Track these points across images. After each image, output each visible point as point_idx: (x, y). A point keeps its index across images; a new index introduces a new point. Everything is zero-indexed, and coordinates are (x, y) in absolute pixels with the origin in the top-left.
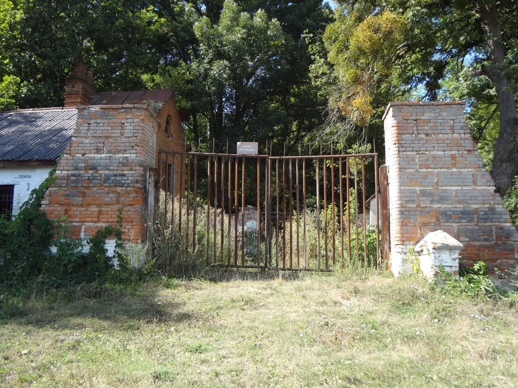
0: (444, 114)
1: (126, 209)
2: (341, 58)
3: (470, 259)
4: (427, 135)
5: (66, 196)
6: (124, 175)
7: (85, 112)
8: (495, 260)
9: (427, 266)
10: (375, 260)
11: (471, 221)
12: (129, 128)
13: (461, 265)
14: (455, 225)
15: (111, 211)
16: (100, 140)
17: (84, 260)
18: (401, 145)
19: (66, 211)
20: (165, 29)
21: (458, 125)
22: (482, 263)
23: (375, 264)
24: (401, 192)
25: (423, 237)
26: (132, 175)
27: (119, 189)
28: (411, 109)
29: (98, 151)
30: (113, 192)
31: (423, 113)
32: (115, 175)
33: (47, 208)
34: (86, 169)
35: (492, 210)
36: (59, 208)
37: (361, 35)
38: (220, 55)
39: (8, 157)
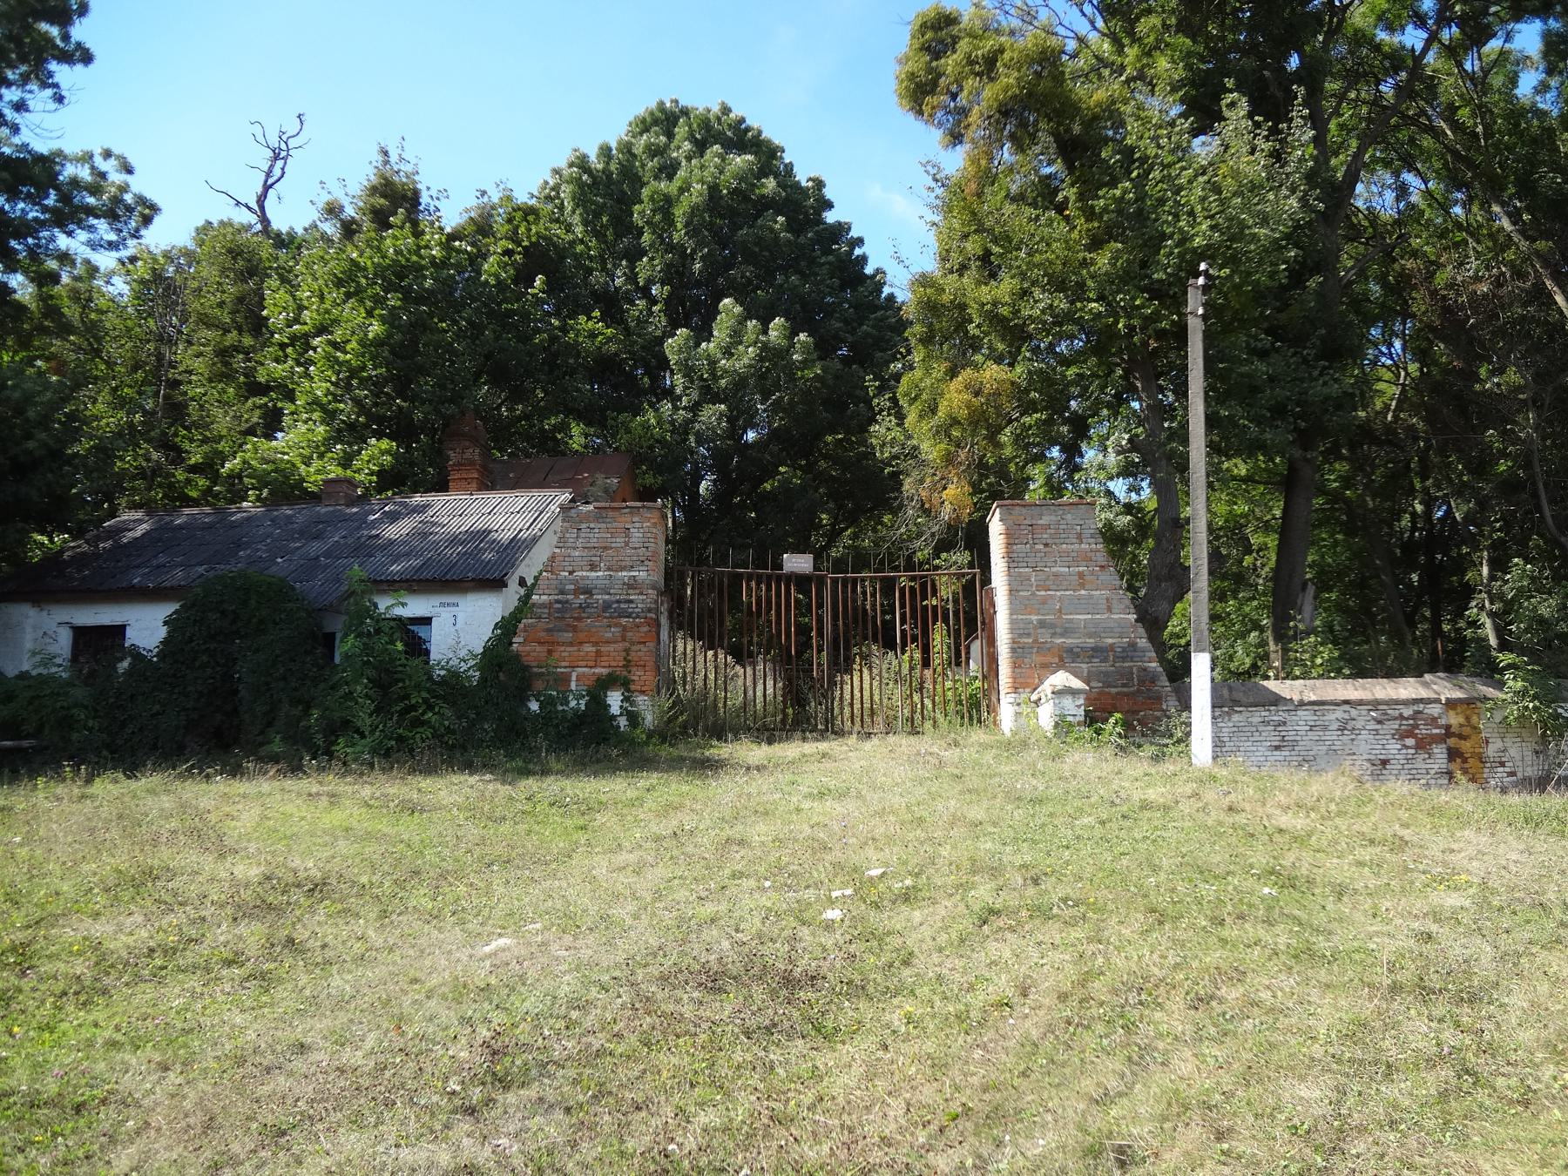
2: (925, 426)
3: (1104, 711)
4: (1046, 545)
5: (548, 630)
6: (631, 601)
8: (1137, 712)
9: (1046, 716)
11: (1105, 660)
12: (636, 536)
14: (1084, 666)
15: (614, 652)
16: (594, 552)
17: (580, 719)
18: (1011, 559)
20: (613, 348)
22: (1118, 715)
23: (979, 721)
24: (1012, 622)
26: (641, 601)
27: (624, 621)
28: (1024, 510)
29: (593, 567)
30: (616, 625)
31: (1041, 516)
32: (618, 602)
34: (577, 592)
35: (1133, 645)
37: (955, 398)
38: (709, 394)
39: (425, 575)
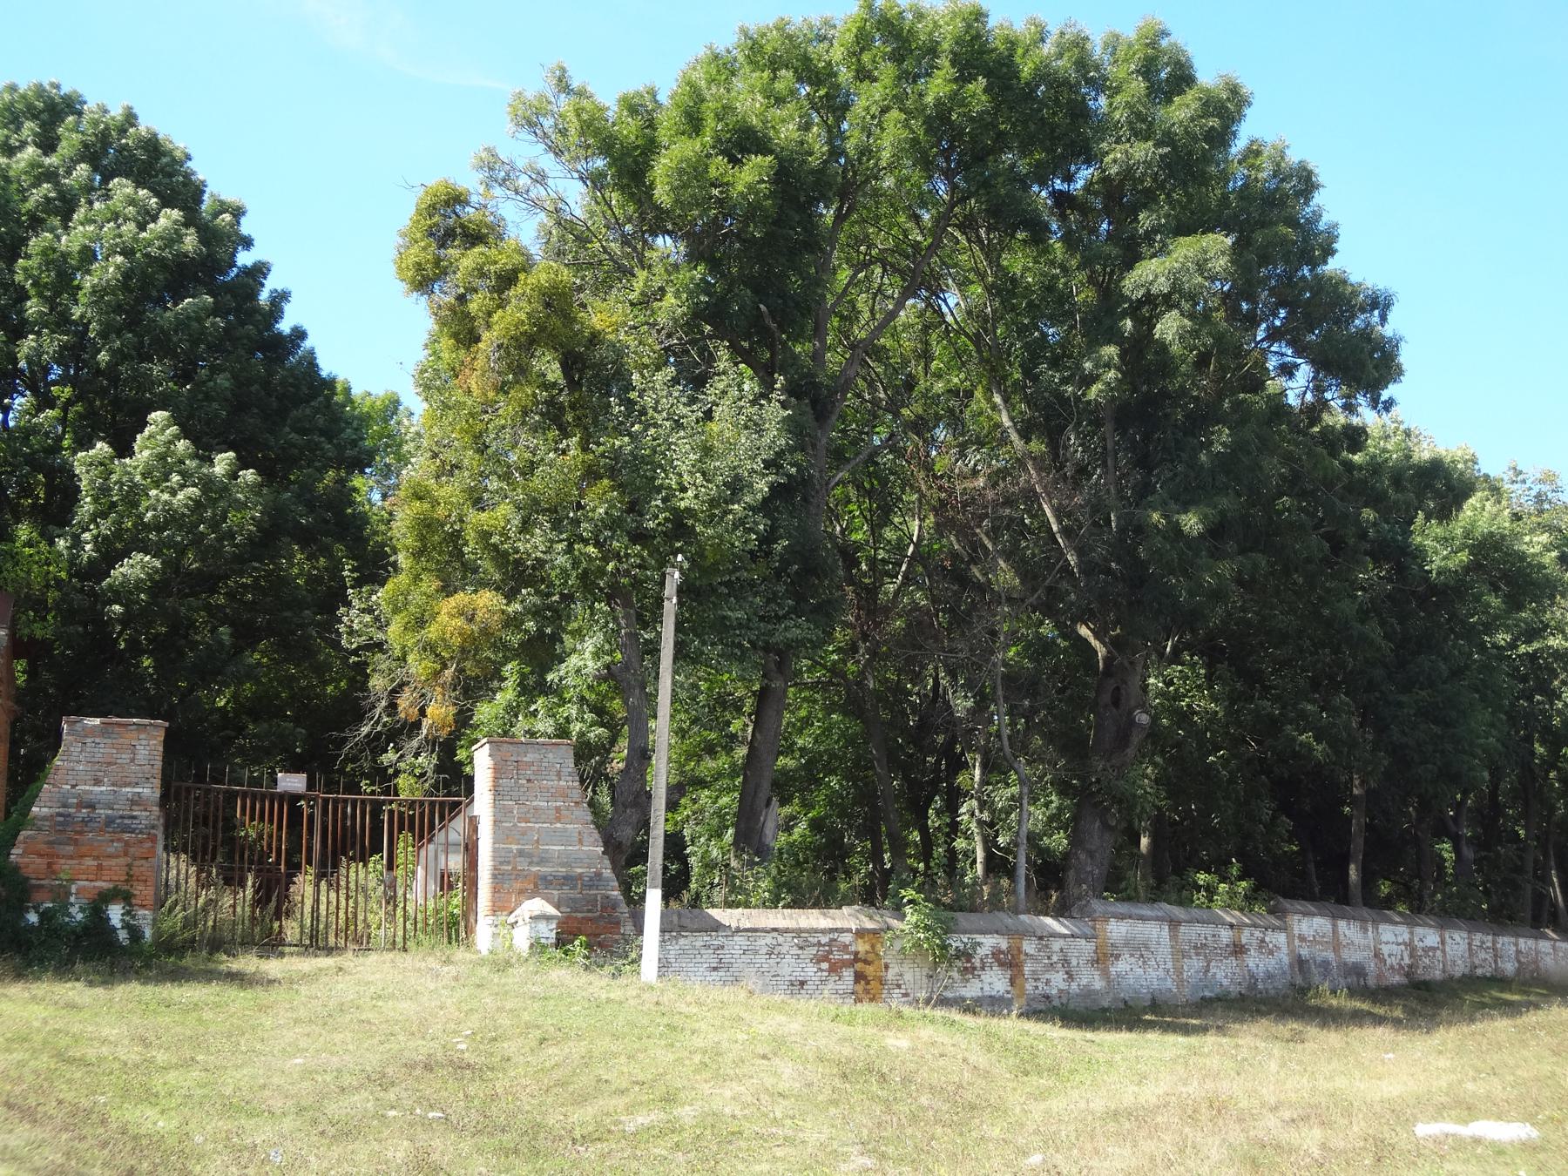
0: (551, 755)
1: (137, 863)
4: (529, 781)
5: (49, 843)
6: (134, 817)
7: (78, 727)
8: (598, 935)
9: (521, 939)
10: (457, 936)
13: (558, 940)
19: (49, 865)
21: (566, 771)
24: (495, 850)
25: (518, 905)
27: (126, 836)
29: (98, 782)
30: (119, 840)
31: (525, 754)
32: (122, 817)
33: (20, 860)
34: (80, 805)
35: (598, 875)
36: (39, 860)
